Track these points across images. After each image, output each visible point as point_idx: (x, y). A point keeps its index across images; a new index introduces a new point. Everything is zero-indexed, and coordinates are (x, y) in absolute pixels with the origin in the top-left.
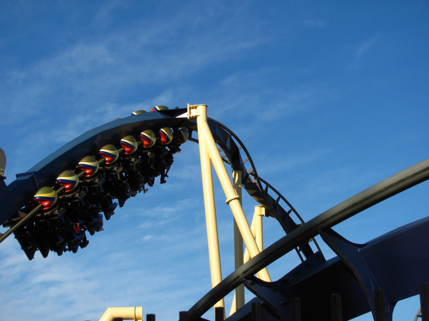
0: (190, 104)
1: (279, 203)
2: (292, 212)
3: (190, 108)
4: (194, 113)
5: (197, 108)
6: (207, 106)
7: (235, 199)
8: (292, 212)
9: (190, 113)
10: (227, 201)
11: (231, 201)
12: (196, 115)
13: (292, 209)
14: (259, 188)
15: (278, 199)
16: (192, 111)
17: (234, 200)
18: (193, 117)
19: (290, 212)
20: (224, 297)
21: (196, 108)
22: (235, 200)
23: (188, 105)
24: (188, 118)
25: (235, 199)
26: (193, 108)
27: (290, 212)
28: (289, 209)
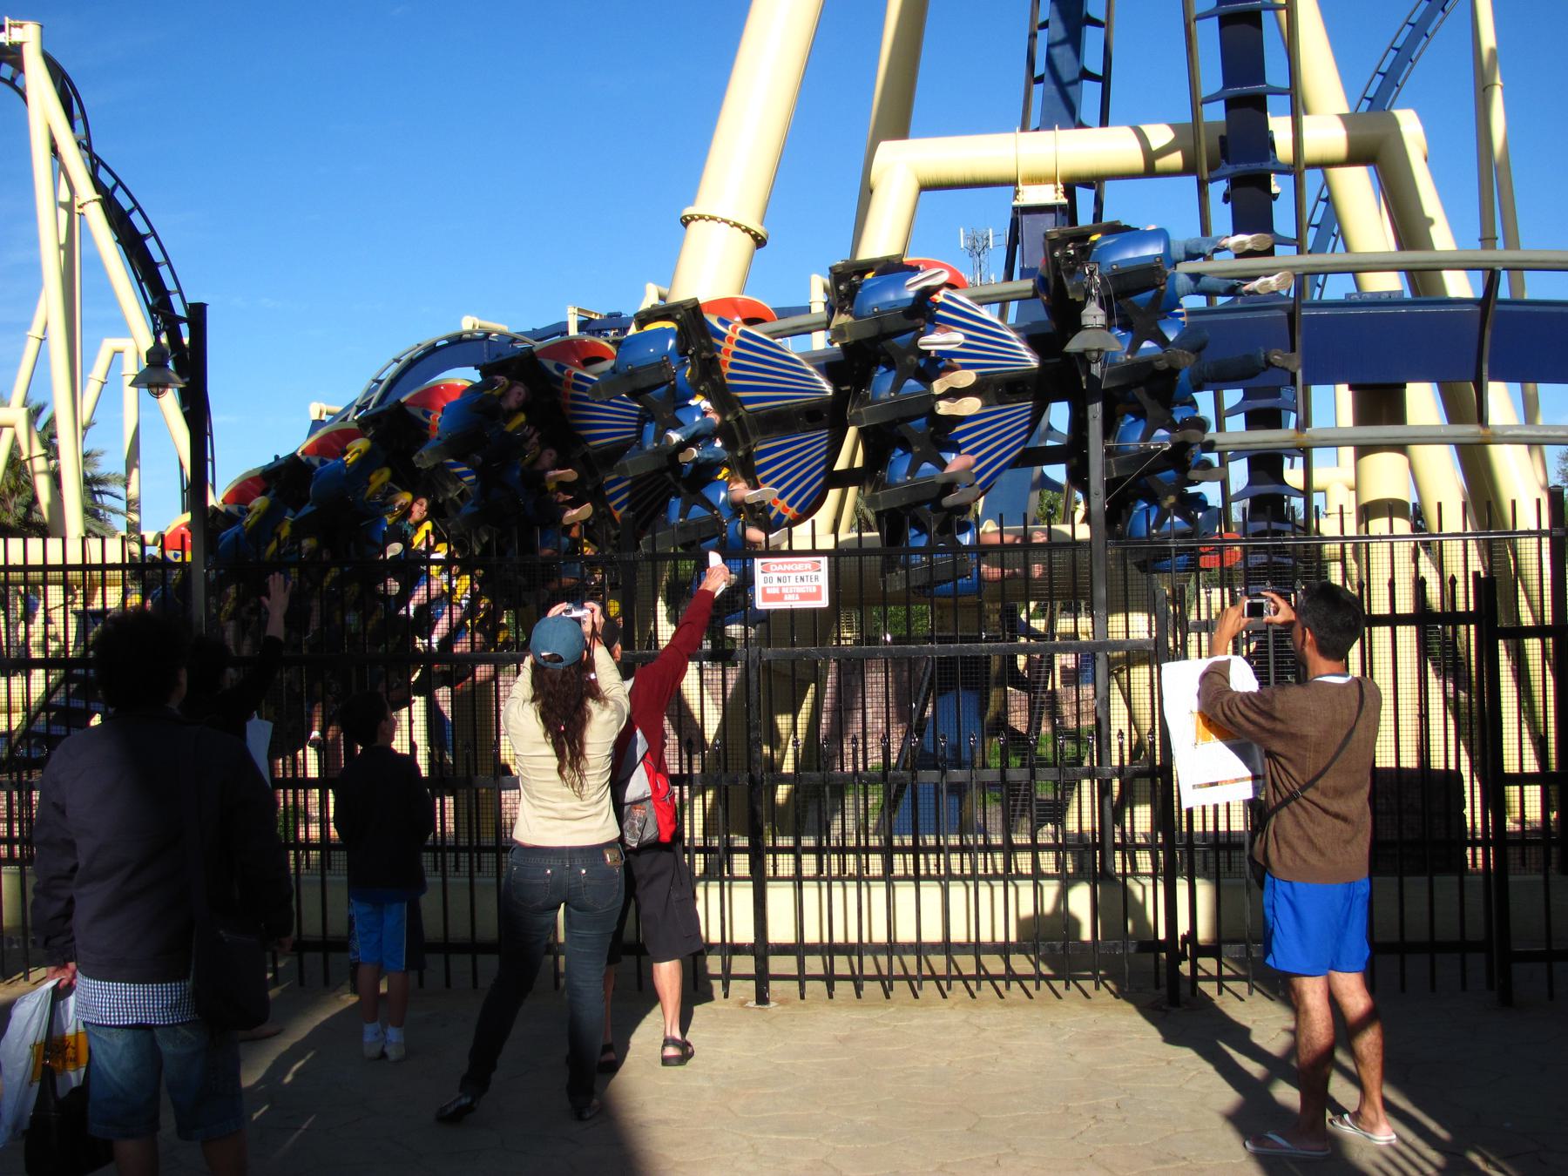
0: (11, 18)
1: (116, 195)
2: (137, 212)
3: (10, 26)
4: (16, 36)
5: (25, 27)
6: (42, 26)
7: (747, 230)
8: (1205, 92)
9: (10, 35)
10: (688, 211)
11: (696, 220)
12: (22, 40)
13: (137, 206)
14: (1484, 647)
15: (114, 188)
16: (14, 30)
17: (744, 231)
18: (15, 43)
19: (131, 211)
20: (153, 260)
21: (21, 26)
22: (747, 234)
23: (7, 19)
24: (7, 44)
25: (95, 200)
26: (16, 26)
27: (131, 211)
28: (132, 205)
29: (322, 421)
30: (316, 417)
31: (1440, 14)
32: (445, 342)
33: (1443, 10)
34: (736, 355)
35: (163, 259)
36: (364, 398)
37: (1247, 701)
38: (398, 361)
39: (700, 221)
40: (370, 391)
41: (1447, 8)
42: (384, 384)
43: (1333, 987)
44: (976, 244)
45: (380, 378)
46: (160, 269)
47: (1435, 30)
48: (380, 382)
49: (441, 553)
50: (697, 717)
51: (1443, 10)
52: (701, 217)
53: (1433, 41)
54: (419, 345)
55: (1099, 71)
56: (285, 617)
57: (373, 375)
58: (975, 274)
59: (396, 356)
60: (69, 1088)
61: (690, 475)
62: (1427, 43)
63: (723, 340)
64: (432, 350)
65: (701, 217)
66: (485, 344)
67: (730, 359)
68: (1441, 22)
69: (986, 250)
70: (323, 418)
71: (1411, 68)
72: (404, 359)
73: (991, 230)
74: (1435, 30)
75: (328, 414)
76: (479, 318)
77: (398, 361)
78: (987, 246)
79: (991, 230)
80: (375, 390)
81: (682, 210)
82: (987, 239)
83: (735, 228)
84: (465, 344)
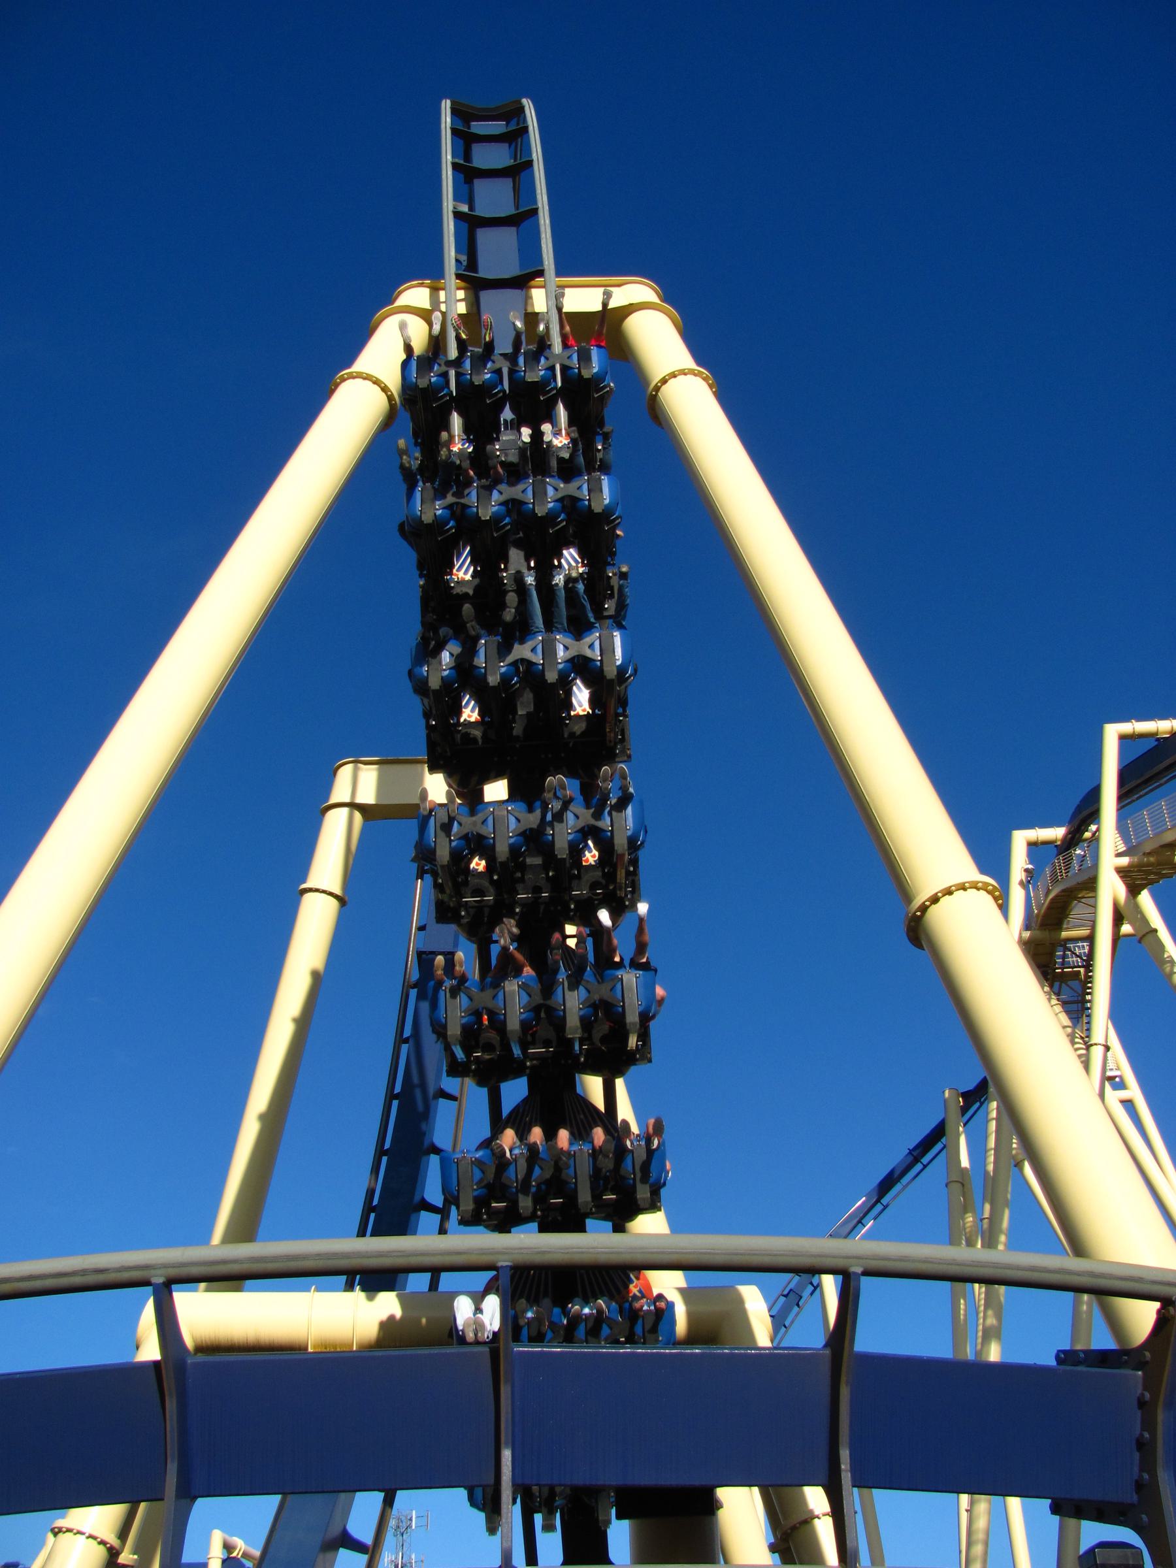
7: (102, 1542)
31: (796, 1309)
33: (798, 1305)
37: (1154, 827)
39: (67, 1533)
41: (801, 1303)
44: (401, 1524)
47: (792, 1322)
49: (537, 1134)
50: (1109, 1021)
51: (798, 1305)
52: (69, 1530)
53: (790, 1332)
55: (367, 1538)
56: (603, 1036)
58: (397, 1554)
62: (786, 1332)
65: (69, 1530)
68: (796, 1315)
69: (409, 1530)
71: (798, 1313)
73: (414, 1512)
74: (792, 1322)
78: (410, 1526)
79: (414, 1512)
81: (53, 1522)
82: (411, 1520)
83: (90, 1540)
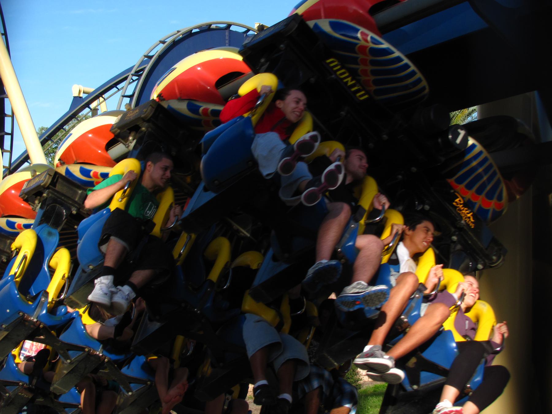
2: (10, 119)
29: (80, 97)
30: (76, 95)
32: (197, 30)
34: (374, 72)
35: (9, 149)
36: (139, 67)
38: (163, 42)
40: (143, 63)
42: (166, 44)
43: (117, 191)
45: (151, 54)
46: (6, 118)
48: (151, 57)
54: (178, 32)
57: (145, 52)
59: (162, 39)
60: (45, 289)
61: (465, 161)
63: (357, 64)
64: (189, 35)
66: (227, 33)
67: (372, 78)
70: (82, 95)
72: (169, 41)
75: (84, 93)
76: (84, 86)
77: (163, 42)
80: (146, 62)
84: (213, 31)
